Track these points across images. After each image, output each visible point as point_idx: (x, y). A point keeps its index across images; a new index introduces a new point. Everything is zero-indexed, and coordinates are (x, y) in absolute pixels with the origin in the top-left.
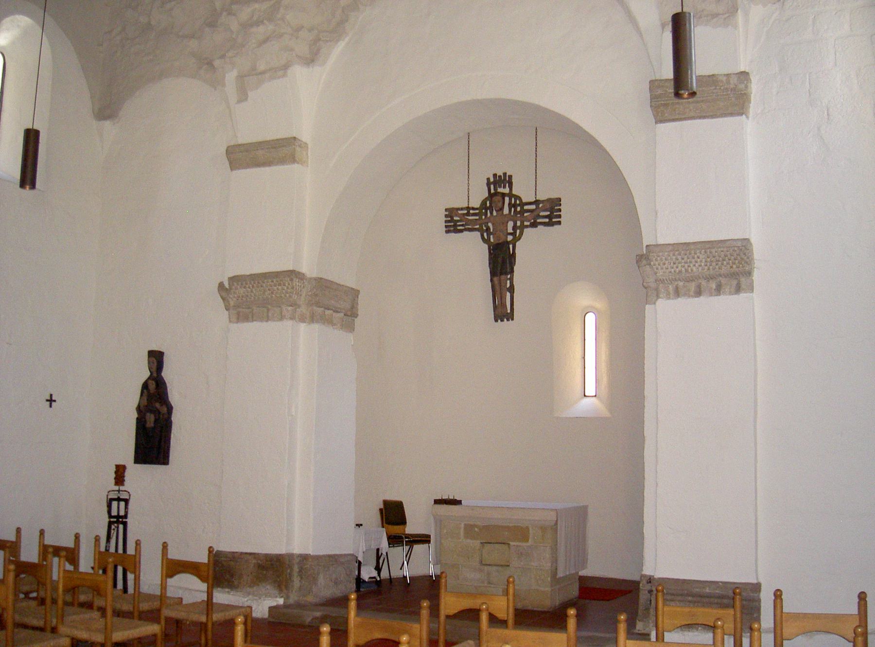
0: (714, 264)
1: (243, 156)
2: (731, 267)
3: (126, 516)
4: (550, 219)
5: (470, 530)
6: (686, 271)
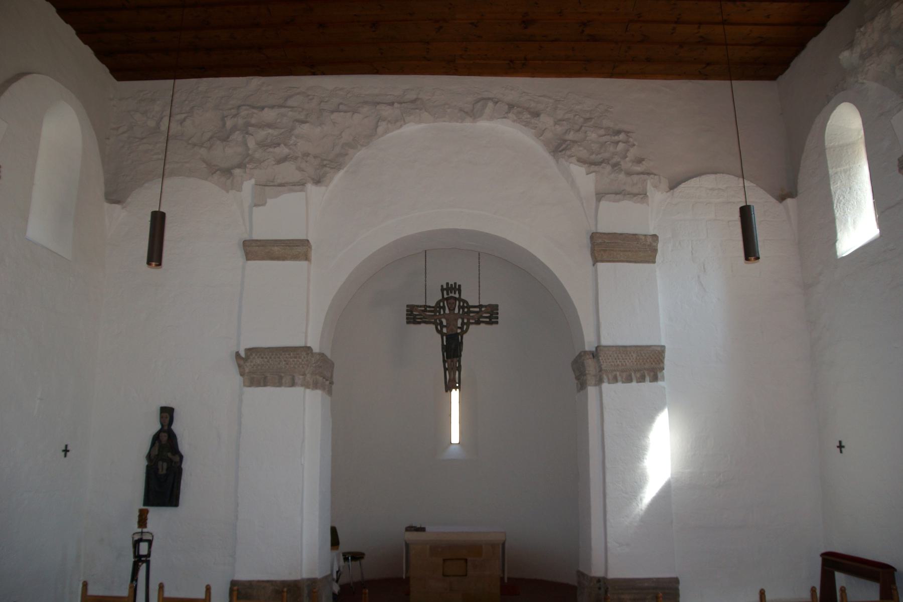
1: (255, 249)
3: (149, 555)
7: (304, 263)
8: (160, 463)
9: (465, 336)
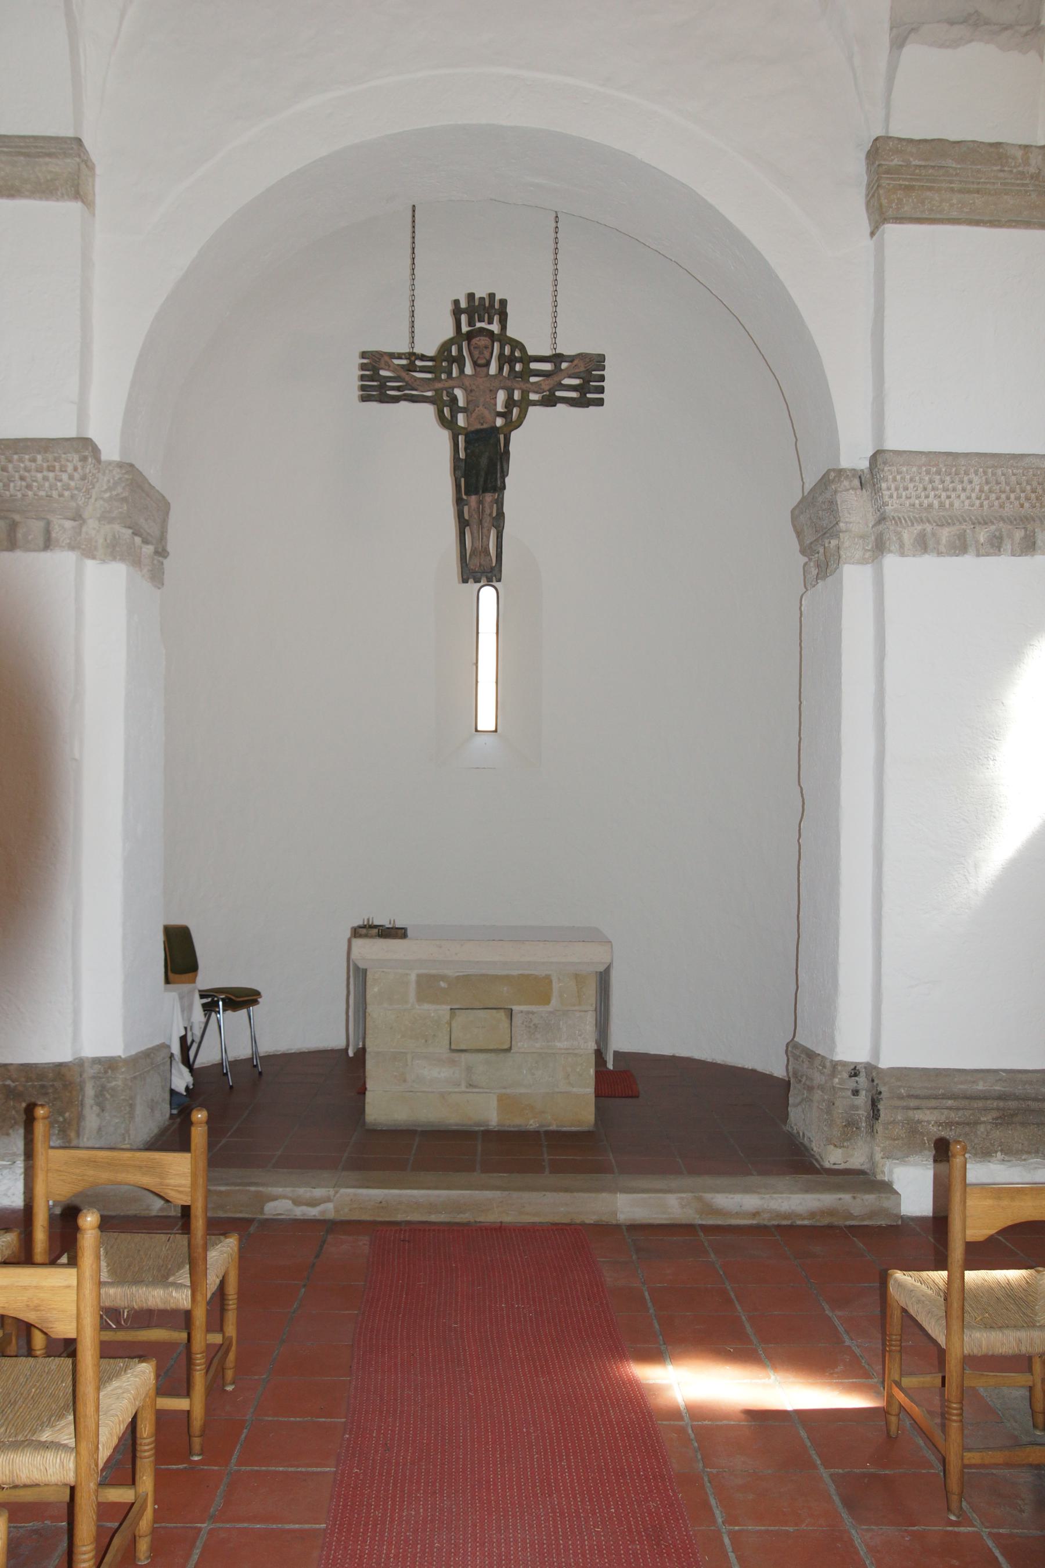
0: (993, 496)
2: (1022, 506)
4: (583, 395)
5: (429, 987)
6: (942, 505)
7: (74, 207)
9: (515, 435)
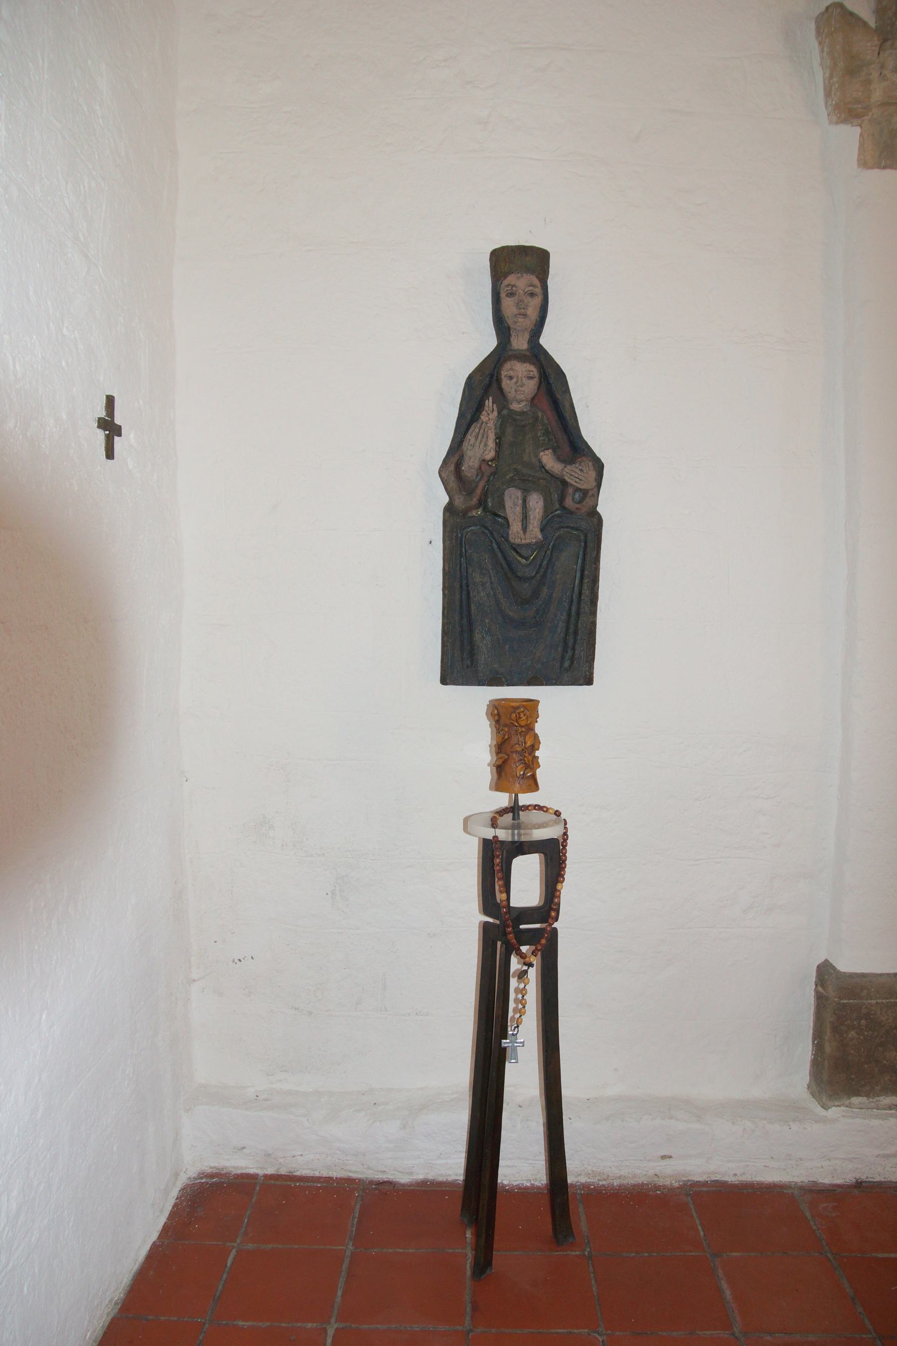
8: (512, 499)
